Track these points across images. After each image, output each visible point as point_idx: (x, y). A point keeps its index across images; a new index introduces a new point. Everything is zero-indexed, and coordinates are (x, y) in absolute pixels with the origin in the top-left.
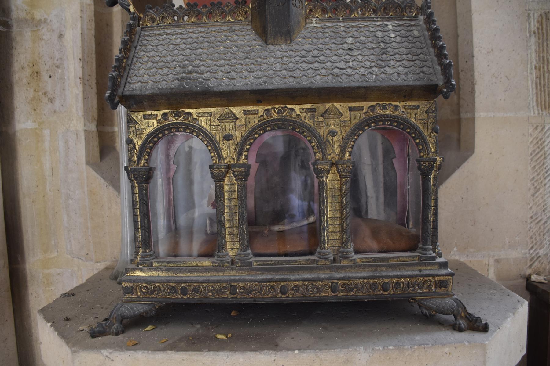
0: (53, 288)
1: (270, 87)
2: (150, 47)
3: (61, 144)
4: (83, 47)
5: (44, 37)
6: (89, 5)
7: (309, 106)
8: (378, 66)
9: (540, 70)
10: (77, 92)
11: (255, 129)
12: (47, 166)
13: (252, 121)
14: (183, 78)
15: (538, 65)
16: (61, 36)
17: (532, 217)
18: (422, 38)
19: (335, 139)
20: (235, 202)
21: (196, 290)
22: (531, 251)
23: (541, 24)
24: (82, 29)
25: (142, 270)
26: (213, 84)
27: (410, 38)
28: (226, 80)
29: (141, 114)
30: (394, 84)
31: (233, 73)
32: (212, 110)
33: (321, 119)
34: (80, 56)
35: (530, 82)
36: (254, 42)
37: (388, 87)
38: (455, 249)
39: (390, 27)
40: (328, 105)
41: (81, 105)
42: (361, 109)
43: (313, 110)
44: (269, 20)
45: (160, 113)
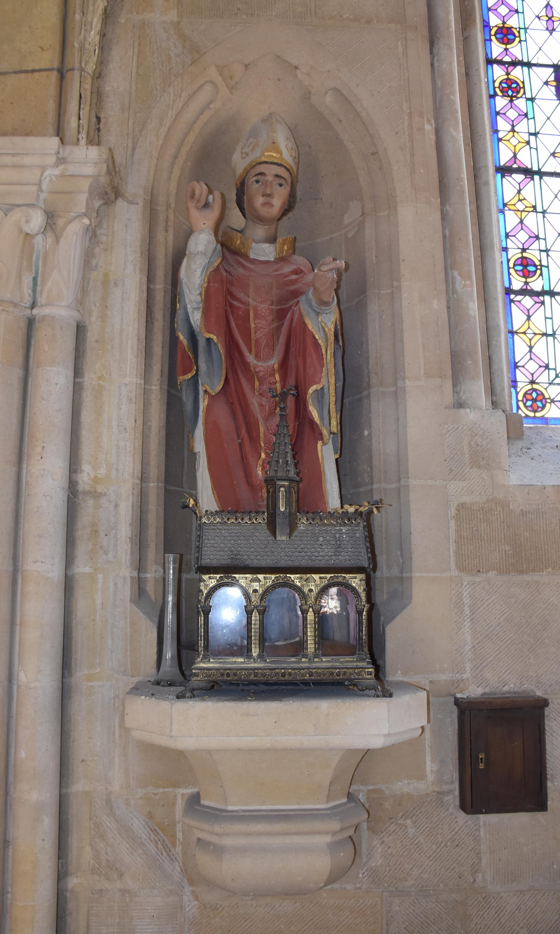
0: (93, 698)
1: (279, 566)
2: (210, 537)
3: (111, 585)
4: (133, 515)
5: (104, 506)
6: (138, 484)
7: (298, 576)
8: (336, 555)
9: (458, 543)
10: (127, 548)
11: (269, 587)
12: (99, 601)
13: (268, 582)
14: (232, 558)
15: (457, 540)
16: (116, 506)
17: (456, 650)
18: (361, 539)
19: (312, 593)
20: (258, 626)
21: (235, 674)
22: (457, 675)
23: (459, 511)
24: (133, 502)
25: (204, 663)
26: (248, 562)
27: (354, 538)
28: (255, 561)
29: (207, 576)
30: (343, 566)
31: (259, 557)
32: (248, 575)
33: (305, 583)
34: (130, 522)
35: (451, 552)
36: (269, 538)
37: (340, 567)
38: (399, 672)
39: (344, 531)
40: (308, 575)
41: (128, 557)
42: (326, 578)
43: (301, 578)
44: (277, 526)
45: (218, 576)
